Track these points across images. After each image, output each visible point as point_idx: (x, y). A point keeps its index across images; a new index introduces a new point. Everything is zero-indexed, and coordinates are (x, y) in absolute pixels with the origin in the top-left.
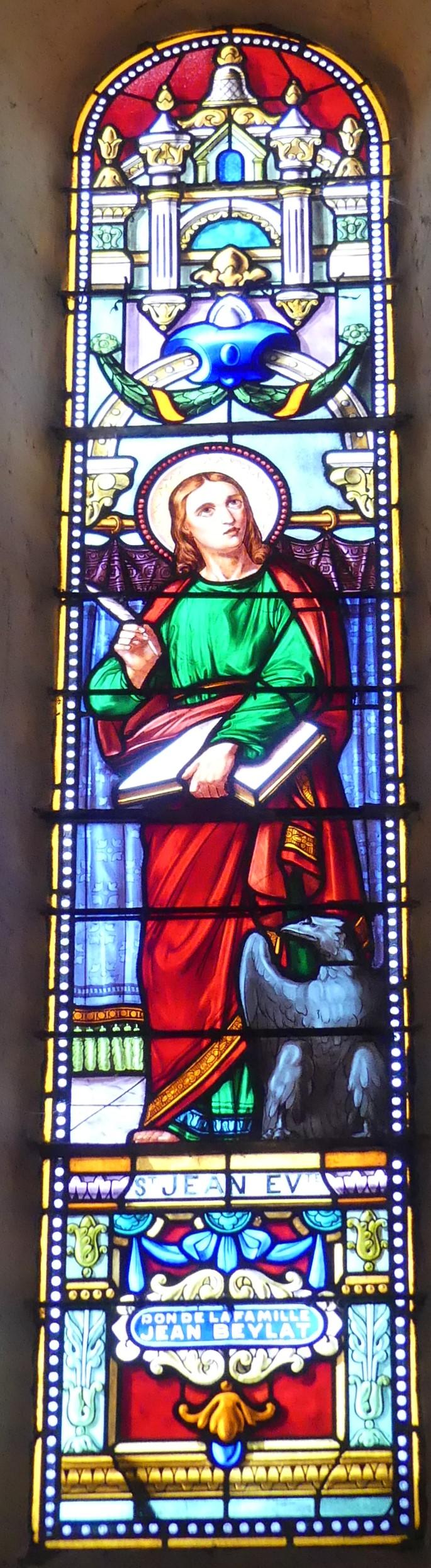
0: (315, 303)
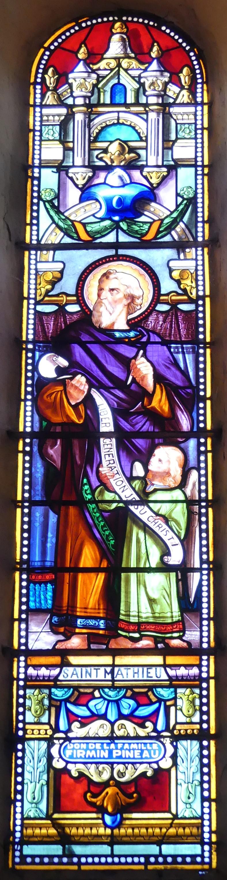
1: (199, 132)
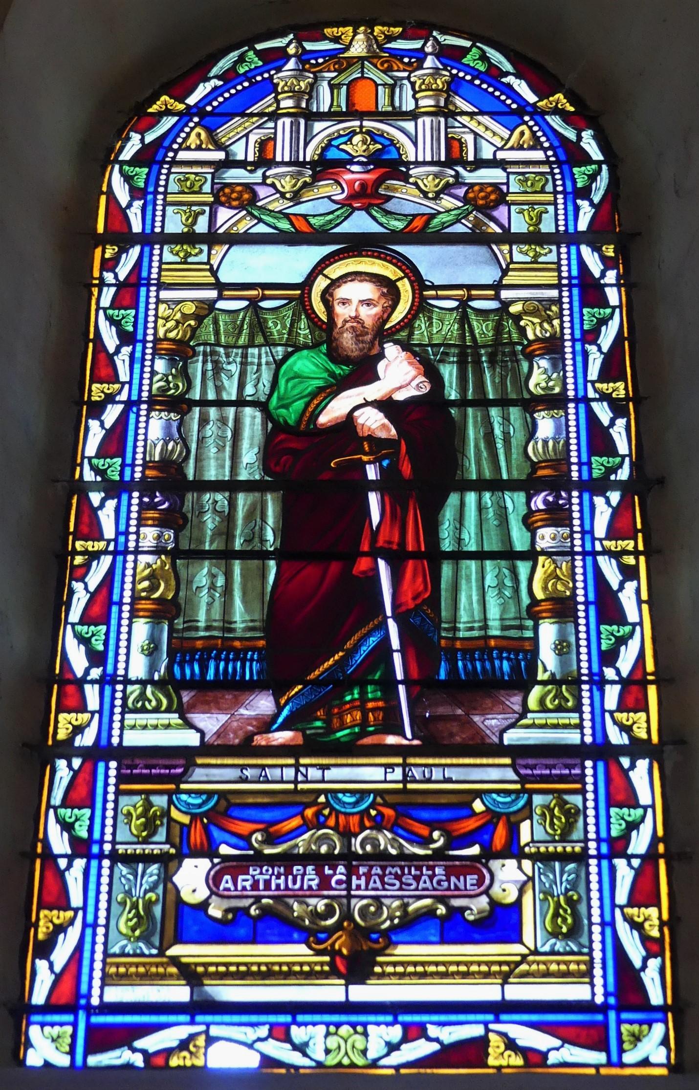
0: (308, 179)
1: (560, 196)
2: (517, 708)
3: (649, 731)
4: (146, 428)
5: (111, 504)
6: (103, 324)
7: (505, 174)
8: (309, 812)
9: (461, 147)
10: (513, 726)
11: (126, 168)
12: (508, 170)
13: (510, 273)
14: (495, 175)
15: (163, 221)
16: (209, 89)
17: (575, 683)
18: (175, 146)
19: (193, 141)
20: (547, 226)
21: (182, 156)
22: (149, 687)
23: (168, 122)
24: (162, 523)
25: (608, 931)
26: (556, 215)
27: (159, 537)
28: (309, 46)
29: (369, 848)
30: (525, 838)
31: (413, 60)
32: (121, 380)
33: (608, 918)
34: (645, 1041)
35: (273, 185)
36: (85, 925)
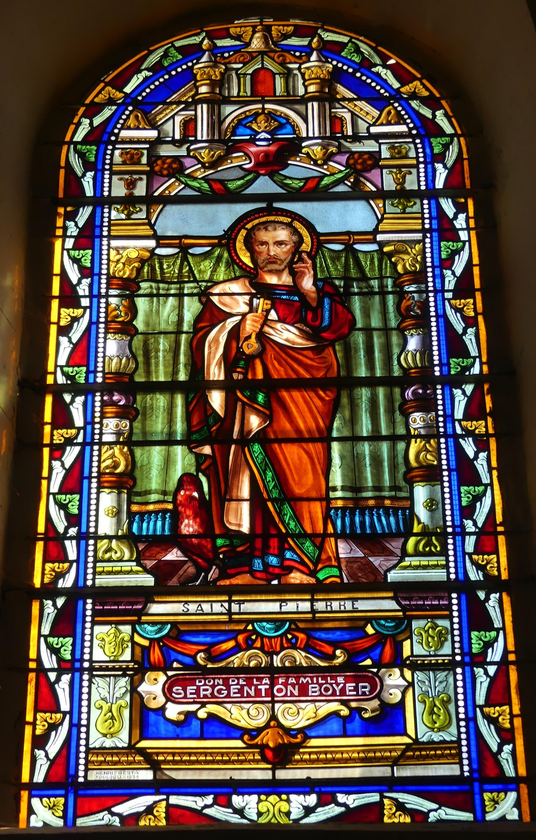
2: (398, 552)
3: (499, 570)
4: (104, 348)
5: (80, 399)
6: (54, 510)
7: (378, 145)
8: (241, 638)
9: (342, 124)
10: (394, 567)
11: (79, 147)
12: (380, 141)
13: (385, 221)
14: (370, 146)
15: (110, 187)
16: (141, 79)
17: (443, 536)
18: (116, 131)
19: (131, 122)
20: (411, 184)
21: (124, 134)
22: (114, 541)
23: (107, 113)
24: (119, 415)
25: (471, 724)
26: (419, 177)
27: (117, 425)
28: (220, 43)
29: (287, 664)
30: (406, 652)
31: (303, 54)
32: (76, 425)
33: (471, 715)
34: (502, 803)
35: (195, 157)
36: (71, 725)
